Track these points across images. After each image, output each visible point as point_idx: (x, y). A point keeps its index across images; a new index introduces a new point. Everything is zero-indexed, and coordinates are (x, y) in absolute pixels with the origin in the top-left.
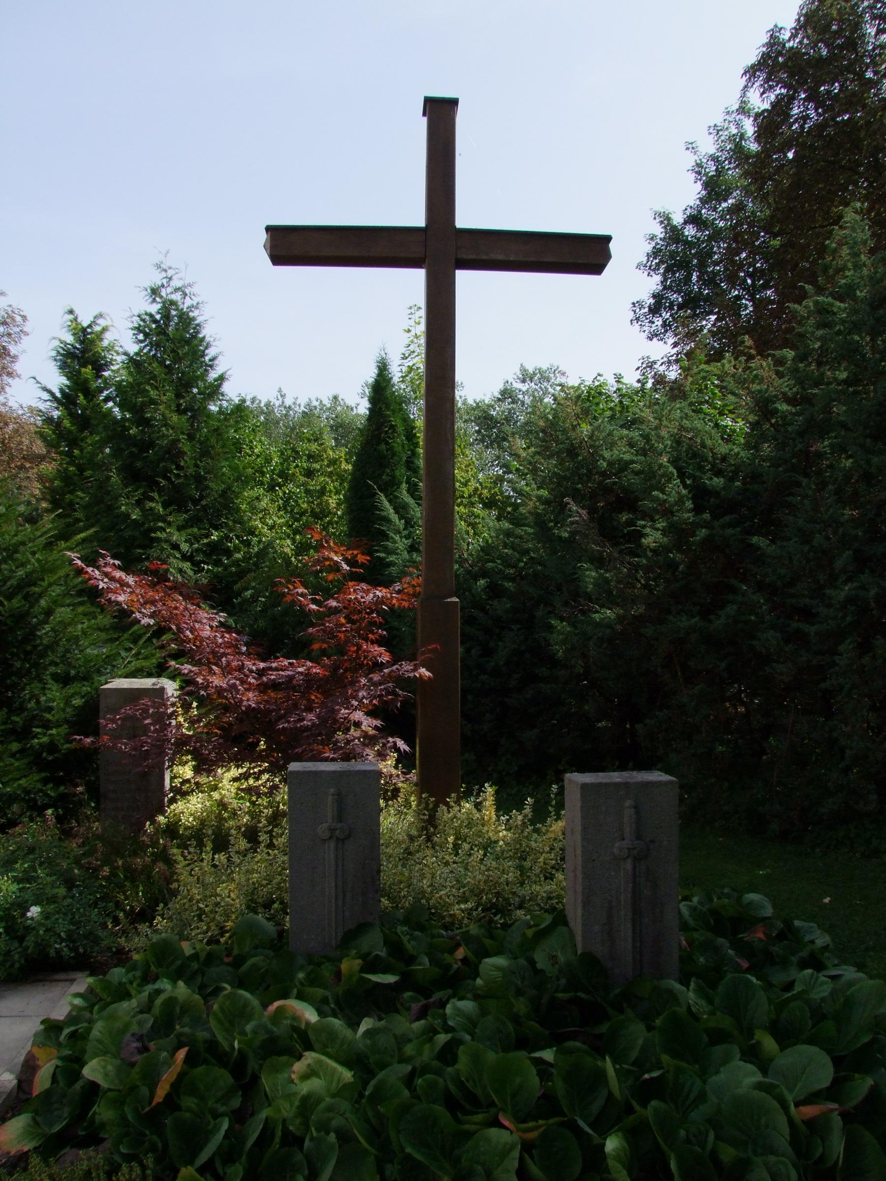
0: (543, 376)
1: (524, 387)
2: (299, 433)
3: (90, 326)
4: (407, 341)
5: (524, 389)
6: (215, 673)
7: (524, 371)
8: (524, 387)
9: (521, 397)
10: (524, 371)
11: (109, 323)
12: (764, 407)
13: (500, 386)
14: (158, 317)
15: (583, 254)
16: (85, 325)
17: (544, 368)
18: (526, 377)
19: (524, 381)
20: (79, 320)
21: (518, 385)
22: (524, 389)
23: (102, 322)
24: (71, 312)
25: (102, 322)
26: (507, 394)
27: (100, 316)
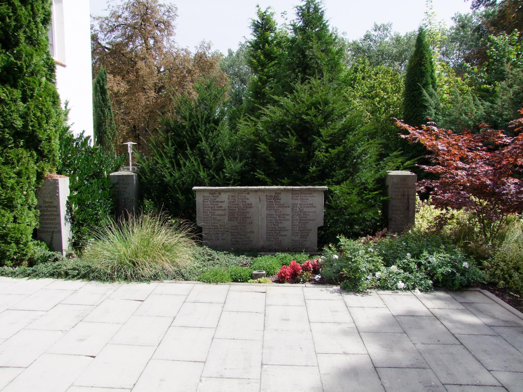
0: (385, 28)
1: (376, 34)
2: (233, 60)
3: (265, 12)
4: (423, 18)
5: (376, 34)
6: (33, 158)
7: (376, 26)
8: (376, 34)
9: (374, 38)
10: (376, 26)
11: (273, 11)
12: (435, 208)
13: (364, 33)
14: (304, 8)
15: (289, 207)
16: (263, 12)
17: (385, 24)
18: (377, 28)
19: (376, 30)
20: (261, 10)
21: (373, 33)
22: (376, 34)
23: (270, 11)
24: (258, 6)
25: (270, 11)
26: (367, 37)
27: (269, 8)
